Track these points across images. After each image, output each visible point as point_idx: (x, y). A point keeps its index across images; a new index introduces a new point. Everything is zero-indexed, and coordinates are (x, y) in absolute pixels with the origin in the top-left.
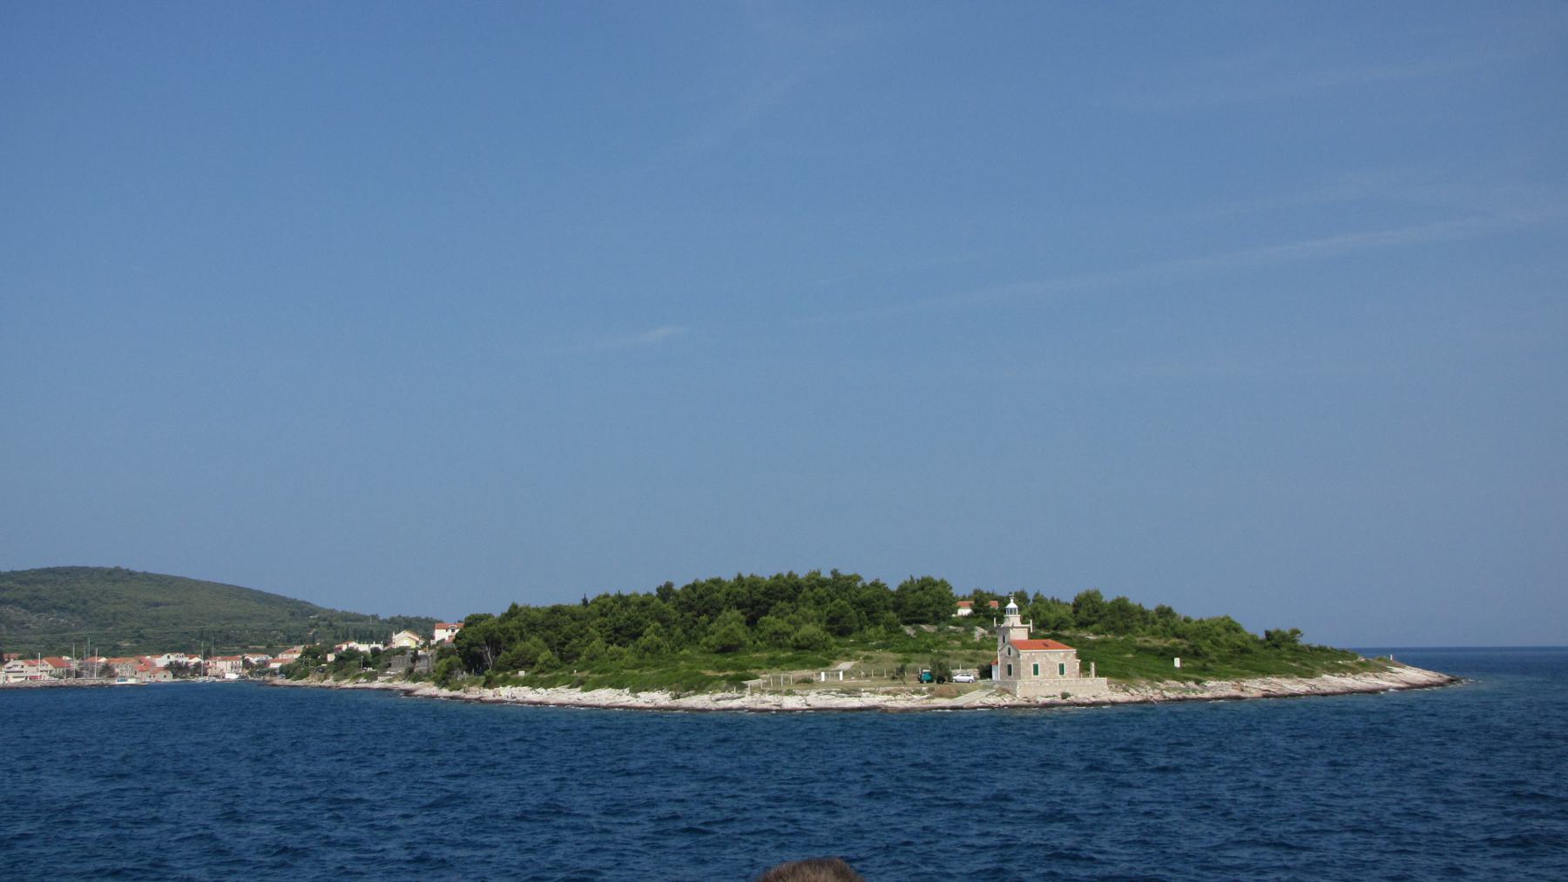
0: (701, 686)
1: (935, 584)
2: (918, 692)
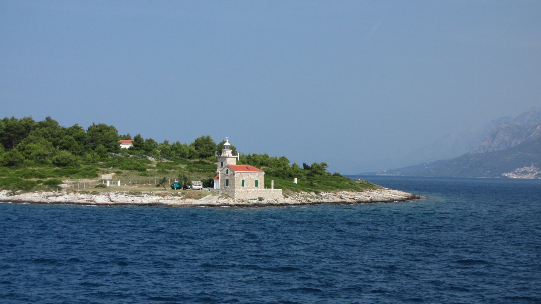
0: (28, 188)
1: (108, 129)
2: (177, 195)
